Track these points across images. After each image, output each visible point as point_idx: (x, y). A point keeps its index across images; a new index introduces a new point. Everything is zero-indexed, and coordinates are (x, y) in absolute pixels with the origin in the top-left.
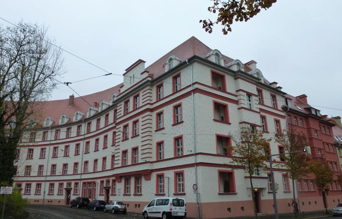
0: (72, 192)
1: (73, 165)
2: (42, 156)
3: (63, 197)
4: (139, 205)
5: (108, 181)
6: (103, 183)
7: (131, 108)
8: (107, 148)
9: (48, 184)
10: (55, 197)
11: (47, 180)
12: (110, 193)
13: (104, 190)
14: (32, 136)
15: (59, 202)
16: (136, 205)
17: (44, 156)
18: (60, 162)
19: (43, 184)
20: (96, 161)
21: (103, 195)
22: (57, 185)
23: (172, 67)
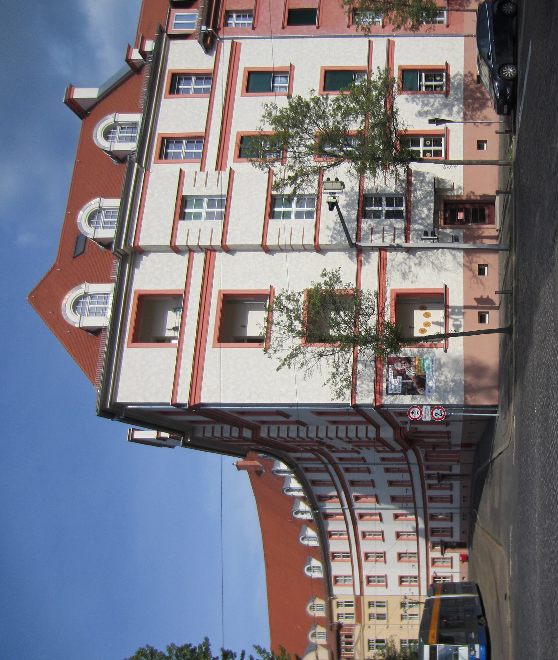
0: (447, 539)
1: (392, 488)
2: (383, 580)
3: (456, 484)
4: (464, 497)
5: (429, 477)
6: (432, 485)
7: (325, 476)
8: (372, 481)
9: (429, 505)
10: (456, 492)
11: (416, 462)
12: (447, 472)
13: (443, 482)
14: (211, 205)
15: (463, 532)
16: (464, 501)
17: (383, 577)
18: (393, 570)
19: (430, 511)
20: (391, 483)
21: (451, 484)
22: (429, 493)
23: (299, 490)
